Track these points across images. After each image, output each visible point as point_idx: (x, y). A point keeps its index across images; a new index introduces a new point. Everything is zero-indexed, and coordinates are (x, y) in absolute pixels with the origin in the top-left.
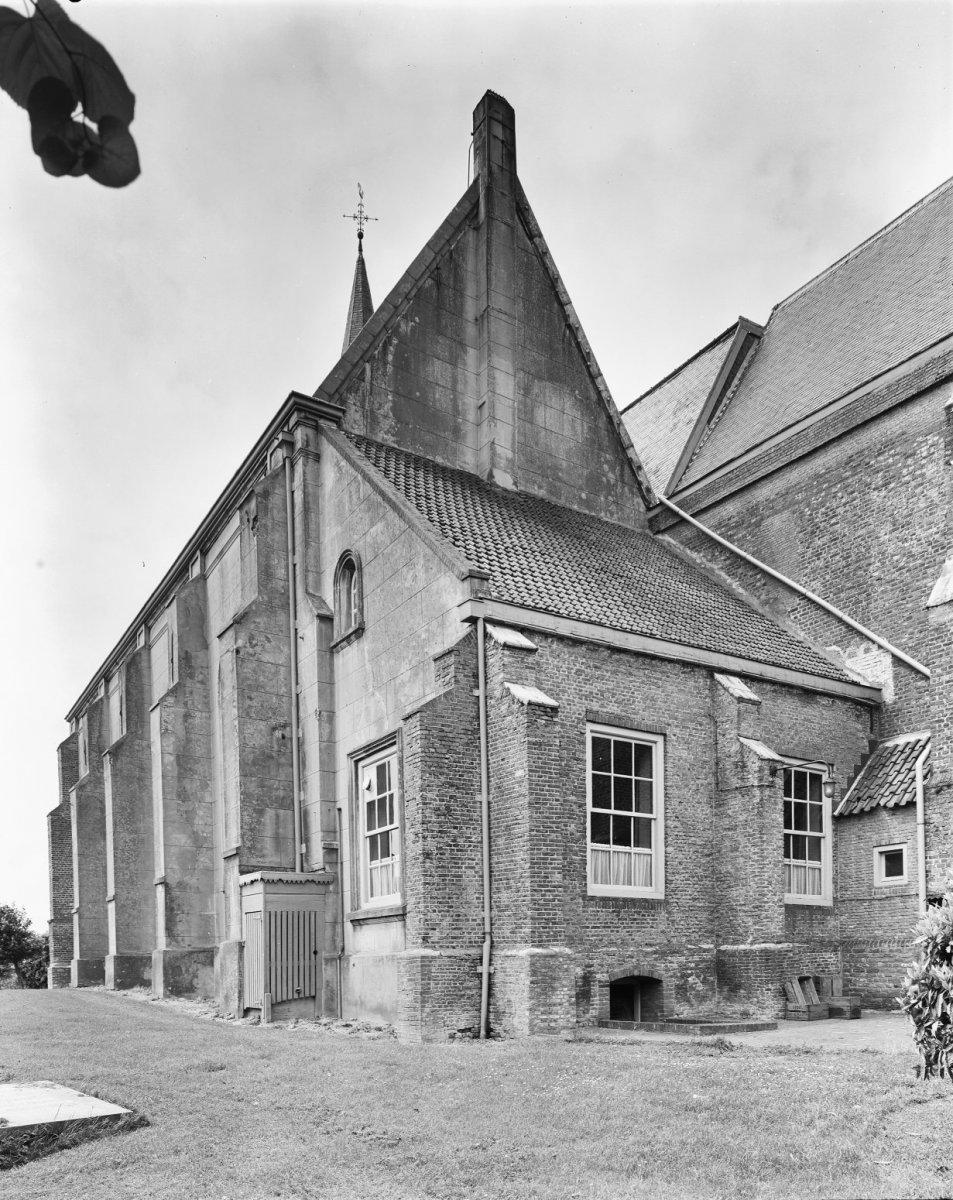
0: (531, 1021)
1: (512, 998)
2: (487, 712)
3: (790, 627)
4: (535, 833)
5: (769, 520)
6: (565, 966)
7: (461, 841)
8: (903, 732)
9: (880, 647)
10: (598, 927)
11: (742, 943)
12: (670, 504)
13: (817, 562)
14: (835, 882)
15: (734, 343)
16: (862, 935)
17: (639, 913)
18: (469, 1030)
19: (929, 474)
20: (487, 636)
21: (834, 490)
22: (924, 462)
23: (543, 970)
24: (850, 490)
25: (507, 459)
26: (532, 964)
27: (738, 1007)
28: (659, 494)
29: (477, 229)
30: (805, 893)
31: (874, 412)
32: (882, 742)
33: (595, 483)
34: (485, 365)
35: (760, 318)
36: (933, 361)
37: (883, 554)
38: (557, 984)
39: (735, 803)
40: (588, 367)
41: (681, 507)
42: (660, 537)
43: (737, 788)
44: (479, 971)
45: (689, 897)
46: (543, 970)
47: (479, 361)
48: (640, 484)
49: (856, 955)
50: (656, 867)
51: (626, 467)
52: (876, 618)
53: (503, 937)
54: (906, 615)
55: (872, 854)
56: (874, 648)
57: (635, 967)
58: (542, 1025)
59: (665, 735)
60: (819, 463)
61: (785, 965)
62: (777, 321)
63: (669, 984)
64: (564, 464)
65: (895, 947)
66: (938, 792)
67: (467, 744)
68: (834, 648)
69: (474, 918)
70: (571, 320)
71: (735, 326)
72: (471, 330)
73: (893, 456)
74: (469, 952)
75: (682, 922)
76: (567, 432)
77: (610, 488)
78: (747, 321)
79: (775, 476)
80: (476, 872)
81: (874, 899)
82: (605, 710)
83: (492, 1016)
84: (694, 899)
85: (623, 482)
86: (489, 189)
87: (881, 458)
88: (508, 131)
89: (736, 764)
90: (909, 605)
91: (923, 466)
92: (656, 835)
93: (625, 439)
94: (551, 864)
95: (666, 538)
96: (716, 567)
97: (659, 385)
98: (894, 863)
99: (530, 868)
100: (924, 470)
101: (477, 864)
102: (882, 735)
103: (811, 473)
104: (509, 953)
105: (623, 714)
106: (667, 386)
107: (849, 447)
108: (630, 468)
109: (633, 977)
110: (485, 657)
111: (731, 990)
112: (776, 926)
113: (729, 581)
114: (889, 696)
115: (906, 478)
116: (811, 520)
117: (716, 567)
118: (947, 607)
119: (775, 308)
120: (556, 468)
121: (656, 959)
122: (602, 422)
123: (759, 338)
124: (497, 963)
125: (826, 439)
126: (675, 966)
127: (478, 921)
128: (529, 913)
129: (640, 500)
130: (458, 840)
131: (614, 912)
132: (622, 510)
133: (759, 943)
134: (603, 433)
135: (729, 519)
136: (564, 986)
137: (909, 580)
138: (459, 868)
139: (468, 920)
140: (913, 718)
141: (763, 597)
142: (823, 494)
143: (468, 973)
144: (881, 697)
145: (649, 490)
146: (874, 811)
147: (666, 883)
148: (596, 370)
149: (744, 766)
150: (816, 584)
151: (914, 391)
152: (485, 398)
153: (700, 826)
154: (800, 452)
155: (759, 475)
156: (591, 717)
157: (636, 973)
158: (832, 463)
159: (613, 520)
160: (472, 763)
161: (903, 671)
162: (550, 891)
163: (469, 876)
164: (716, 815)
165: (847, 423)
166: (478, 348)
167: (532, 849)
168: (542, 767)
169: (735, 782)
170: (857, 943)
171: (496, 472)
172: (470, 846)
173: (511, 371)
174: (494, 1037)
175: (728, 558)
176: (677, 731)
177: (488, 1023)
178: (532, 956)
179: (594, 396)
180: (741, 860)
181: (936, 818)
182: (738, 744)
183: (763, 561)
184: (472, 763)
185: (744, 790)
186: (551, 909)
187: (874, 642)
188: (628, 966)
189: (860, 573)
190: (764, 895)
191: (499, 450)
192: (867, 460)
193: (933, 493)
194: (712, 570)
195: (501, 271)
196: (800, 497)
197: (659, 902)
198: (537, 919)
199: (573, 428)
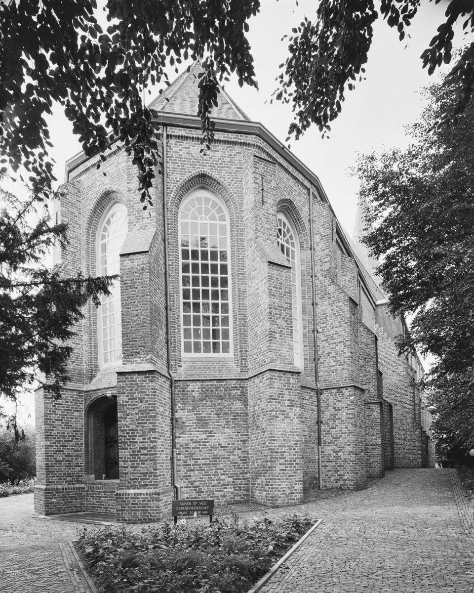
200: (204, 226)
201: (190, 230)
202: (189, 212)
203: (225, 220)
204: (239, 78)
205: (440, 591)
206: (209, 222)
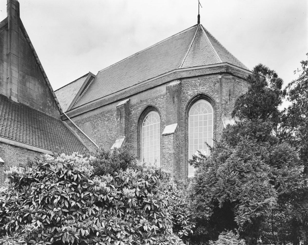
5: (86, 123)
12: (65, 114)
15: (88, 78)
21: (98, 119)
25: (16, 94)
28: (64, 111)
29: (7, 30)
33: (45, 105)
34: (9, 68)
35: (95, 73)
36: (116, 96)
40: (43, 75)
41: (68, 115)
42: (63, 121)
47: (7, 65)
48: (58, 107)
51: (54, 103)
62: (99, 75)
64: (35, 99)
70: (38, 62)
71: (88, 74)
72: (5, 57)
76: (36, 90)
77: (49, 107)
78: (91, 73)
79: (87, 113)
85: (53, 106)
86: (10, 21)
87: (107, 114)
88: (17, 8)
93: (54, 95)
95: (65, 122)
97: (72, 83)
103: (94, 114)
106: (73, 83)
108: (56, 103)
113: (78, 136)
119: (99, 72)
120: (33, 99)
122: (47, 90)
123: (94, 78)
125: (97, 107)
129: (58, 111)
132: (53, 113)
134: (48, 93)
137: (112, 143)
145: (61, 109)
148: (45, 76)
150: (95, 140)
151: (113, 101)
152: (9, 77)
155: (84, 112)
156: (21, 166)
158: (98, 113)
159: (51, 115)
165: (99, 106)
166: (7, 62)
171: (12, 97)
173: (17, 71)
179: (45, 83)
189: (103, 139)
191: (13, 91)
194: (74, 132)
195: (14, 44)
196: (92, 119)
199: (38, 90)
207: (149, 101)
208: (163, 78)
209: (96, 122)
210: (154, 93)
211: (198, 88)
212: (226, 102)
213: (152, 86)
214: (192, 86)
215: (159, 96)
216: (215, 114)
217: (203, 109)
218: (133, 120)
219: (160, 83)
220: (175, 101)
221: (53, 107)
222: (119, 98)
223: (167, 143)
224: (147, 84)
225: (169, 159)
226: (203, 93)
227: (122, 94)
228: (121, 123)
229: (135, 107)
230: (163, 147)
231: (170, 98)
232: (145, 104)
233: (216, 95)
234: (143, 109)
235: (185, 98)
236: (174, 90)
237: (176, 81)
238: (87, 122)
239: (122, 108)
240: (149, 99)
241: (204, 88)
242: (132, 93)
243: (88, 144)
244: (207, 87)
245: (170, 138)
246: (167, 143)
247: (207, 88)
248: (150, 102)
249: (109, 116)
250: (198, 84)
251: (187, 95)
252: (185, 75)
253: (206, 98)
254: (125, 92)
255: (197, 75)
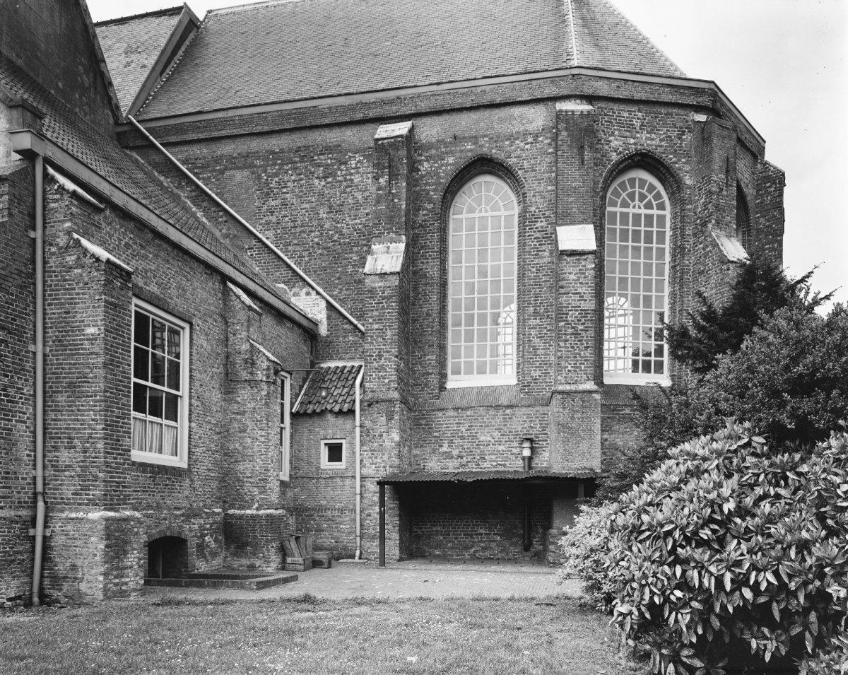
0: (105, 586)
1: (79, 563)
2: (44, 258)
3: (246, 260)
4: (108, 394)
5: (232, 172)
6: (136, 530)
7: (12, 392)
8: (332, 358)
9: (318, 293)
10: (138, 491)
11: (248, 509)
13: (271, 217)
14: (291, 463)
16: (310, 504)
17: (169, 479)
18: (19, 597)
19: (356, 181)
20: (48, 179)
22: (352, 171)
23: (117, 534)
24: (298, 172)
26: (107, 528)
27: (245, 561)
28: (124, 111)
30: (160, 451)
31: (319, 122)
32: (318, 363)
37: (322, 227)
38: (128, 548)
39: (244, 393)
43: (246, 381)
44: (31, 532)
45: (205, 468)
46: (117, 534)
49: (307, 519)
50: (182, 440)
51: (99, 80)
52: (315, 272)
53: (62, 499)
54: (338, 275)
55: (319, 445)
56: (313, 293)
57: (168, 528)
58: (115, 589)
59: (191, 324)
60: (275, 143)
61: (282, 526)
63: (193, 542)
64: (43, 47)
65: (336, 513)
66: (369, 406)
67: (21, 287)
68: (282, 285)
69: (25, 476)
71: (180, 8)
73: (331, 159)
74: (20, 513)
75: (200, 490)
79: (238, 139)
80: (27, 427)
81: (320, 478)
82: (148, 288)
83: (46, 582)
84: (209, 470)
89: (246, 361)
90: (340, 269)
91: (351, 174)
92: (182, 408)
94: (122, 427)
96: (182, 194)
98: (335, 452)
99: (103, 429)
100: (353, 177)
101: (28, 418)
102: (317, 358)
104: (73, 515)
105: (162, 296)
107: (298, 140)
109: (166, 537)
110: (44, 199)
111: (238, 547)
112: (274, 497)
114: (323, 330)
115: (340, 178)
116: (267, 183)
117: (182, 194)
118: (377, 277)
121: (183, 521)
124: (57, 526)
126: (196, 527)
127: (28, 481)
128: (101, 475)
129: (110, 113)
130: (10, 390)
131: (151, 477)
133: (264, 509)
135: (196, 159)
136: (135, 549)
138: (9, 420)
139: (18, 478)
140: (340, 350)
141: (224, 231)
142: (277, 167)
143: (19, 537)
144: (318, 330)
146: (323, 413)
147: (189, 454)
149: (253, 364)
150: (271, 234)
151: (347, 119)
153: (214, 407)
154: (259, 129)
155: (224, 133)
157: (168, 534)
160: (26, 309)
161: (334, 315)
162: (120, 454)
163: (21, 432)
164: (225, 400)
167: (106, 411)
168: (116, 330)
169: (244, 375)
170: (307, 509)
172: (21, 398)
174: (49, 604)
175: (193, 191)
176: (200, 322)
177: (41, 589)
178: (107, 519)
180: (249, 440)
181: (368, 424)
182: (248, 344)
183: (226, 202)
184: (26, 309)
185: (253, 383)
186: (122, 473)
187: (313, 288)
188: (163, 527)
190: (269, 471)
192: (312, 154)
193: (359, 196)
194: (179, 196)
196: (258, 163)
197: (183, 470)
198: (110, 482)
199: (52, 16)
200: (637, 218)
201: (464, 243)
202: (494, 193)
203: (664, 209)
204: (768, 157)
205: (637, 673)
206: (644, 211)
207: (482, 141)
208: (534, 83)
209: (276, 175)
210: (502, 121)
211: (638, 135)
212: (720, 188)
213: (498, 100)
214: (621, 124)
215: (518, 132)
216: (680, 219)
217: (642, 197)
218: (423, 190)
219: (526, 97)
220: (586, 158)
221: (95, 94)
222: (372, 114)
223: (572, 277)
224: (479, 89)
225: (580, 327)
226: (649, 151)
227: (383, 102)
228: (390, 192)
229: (433, 152)
230: (562, 287)
231: (570, 146)
232: (470, 150)
233: (684, 163)
234: (462, 163)
235: (602, 156)
236: (583, 126)
237: (578, 101)
238: (238, 168)
239: (397, 149)
240: (485, 136)
241: (653, 139)
242: (424, 106)
243: (240, 243)
244: (662, 137)
245: (584, 266)
246: (572, 277)
247: (661, 140)
248: (489, 148)
249: (332, 165)
250: (637, 124)
251: (606, 147)
252: (604, 89)
253: (654, 166)
254: (399, 98)
255: (637, 96)
